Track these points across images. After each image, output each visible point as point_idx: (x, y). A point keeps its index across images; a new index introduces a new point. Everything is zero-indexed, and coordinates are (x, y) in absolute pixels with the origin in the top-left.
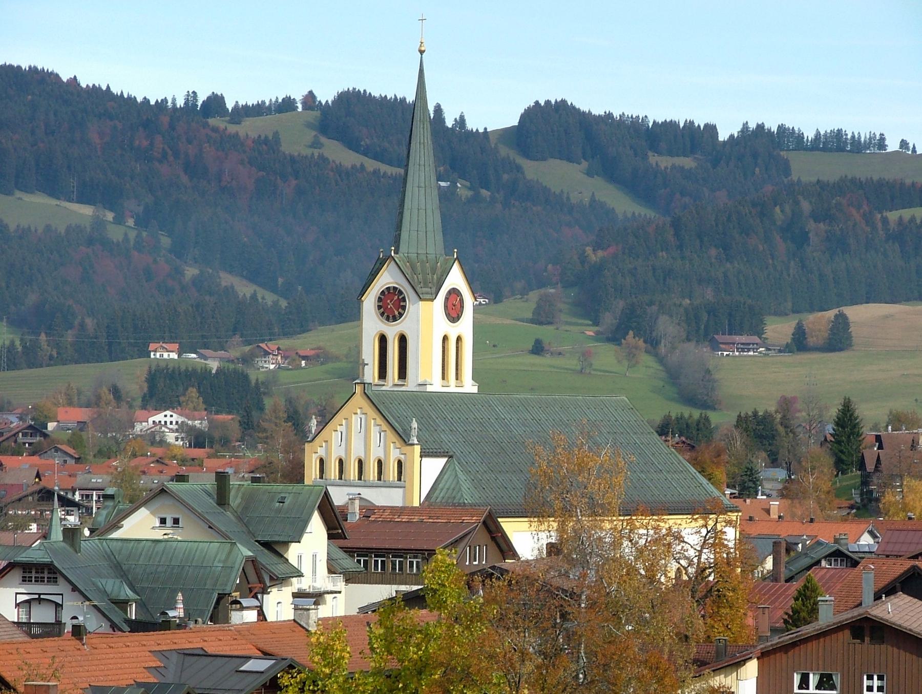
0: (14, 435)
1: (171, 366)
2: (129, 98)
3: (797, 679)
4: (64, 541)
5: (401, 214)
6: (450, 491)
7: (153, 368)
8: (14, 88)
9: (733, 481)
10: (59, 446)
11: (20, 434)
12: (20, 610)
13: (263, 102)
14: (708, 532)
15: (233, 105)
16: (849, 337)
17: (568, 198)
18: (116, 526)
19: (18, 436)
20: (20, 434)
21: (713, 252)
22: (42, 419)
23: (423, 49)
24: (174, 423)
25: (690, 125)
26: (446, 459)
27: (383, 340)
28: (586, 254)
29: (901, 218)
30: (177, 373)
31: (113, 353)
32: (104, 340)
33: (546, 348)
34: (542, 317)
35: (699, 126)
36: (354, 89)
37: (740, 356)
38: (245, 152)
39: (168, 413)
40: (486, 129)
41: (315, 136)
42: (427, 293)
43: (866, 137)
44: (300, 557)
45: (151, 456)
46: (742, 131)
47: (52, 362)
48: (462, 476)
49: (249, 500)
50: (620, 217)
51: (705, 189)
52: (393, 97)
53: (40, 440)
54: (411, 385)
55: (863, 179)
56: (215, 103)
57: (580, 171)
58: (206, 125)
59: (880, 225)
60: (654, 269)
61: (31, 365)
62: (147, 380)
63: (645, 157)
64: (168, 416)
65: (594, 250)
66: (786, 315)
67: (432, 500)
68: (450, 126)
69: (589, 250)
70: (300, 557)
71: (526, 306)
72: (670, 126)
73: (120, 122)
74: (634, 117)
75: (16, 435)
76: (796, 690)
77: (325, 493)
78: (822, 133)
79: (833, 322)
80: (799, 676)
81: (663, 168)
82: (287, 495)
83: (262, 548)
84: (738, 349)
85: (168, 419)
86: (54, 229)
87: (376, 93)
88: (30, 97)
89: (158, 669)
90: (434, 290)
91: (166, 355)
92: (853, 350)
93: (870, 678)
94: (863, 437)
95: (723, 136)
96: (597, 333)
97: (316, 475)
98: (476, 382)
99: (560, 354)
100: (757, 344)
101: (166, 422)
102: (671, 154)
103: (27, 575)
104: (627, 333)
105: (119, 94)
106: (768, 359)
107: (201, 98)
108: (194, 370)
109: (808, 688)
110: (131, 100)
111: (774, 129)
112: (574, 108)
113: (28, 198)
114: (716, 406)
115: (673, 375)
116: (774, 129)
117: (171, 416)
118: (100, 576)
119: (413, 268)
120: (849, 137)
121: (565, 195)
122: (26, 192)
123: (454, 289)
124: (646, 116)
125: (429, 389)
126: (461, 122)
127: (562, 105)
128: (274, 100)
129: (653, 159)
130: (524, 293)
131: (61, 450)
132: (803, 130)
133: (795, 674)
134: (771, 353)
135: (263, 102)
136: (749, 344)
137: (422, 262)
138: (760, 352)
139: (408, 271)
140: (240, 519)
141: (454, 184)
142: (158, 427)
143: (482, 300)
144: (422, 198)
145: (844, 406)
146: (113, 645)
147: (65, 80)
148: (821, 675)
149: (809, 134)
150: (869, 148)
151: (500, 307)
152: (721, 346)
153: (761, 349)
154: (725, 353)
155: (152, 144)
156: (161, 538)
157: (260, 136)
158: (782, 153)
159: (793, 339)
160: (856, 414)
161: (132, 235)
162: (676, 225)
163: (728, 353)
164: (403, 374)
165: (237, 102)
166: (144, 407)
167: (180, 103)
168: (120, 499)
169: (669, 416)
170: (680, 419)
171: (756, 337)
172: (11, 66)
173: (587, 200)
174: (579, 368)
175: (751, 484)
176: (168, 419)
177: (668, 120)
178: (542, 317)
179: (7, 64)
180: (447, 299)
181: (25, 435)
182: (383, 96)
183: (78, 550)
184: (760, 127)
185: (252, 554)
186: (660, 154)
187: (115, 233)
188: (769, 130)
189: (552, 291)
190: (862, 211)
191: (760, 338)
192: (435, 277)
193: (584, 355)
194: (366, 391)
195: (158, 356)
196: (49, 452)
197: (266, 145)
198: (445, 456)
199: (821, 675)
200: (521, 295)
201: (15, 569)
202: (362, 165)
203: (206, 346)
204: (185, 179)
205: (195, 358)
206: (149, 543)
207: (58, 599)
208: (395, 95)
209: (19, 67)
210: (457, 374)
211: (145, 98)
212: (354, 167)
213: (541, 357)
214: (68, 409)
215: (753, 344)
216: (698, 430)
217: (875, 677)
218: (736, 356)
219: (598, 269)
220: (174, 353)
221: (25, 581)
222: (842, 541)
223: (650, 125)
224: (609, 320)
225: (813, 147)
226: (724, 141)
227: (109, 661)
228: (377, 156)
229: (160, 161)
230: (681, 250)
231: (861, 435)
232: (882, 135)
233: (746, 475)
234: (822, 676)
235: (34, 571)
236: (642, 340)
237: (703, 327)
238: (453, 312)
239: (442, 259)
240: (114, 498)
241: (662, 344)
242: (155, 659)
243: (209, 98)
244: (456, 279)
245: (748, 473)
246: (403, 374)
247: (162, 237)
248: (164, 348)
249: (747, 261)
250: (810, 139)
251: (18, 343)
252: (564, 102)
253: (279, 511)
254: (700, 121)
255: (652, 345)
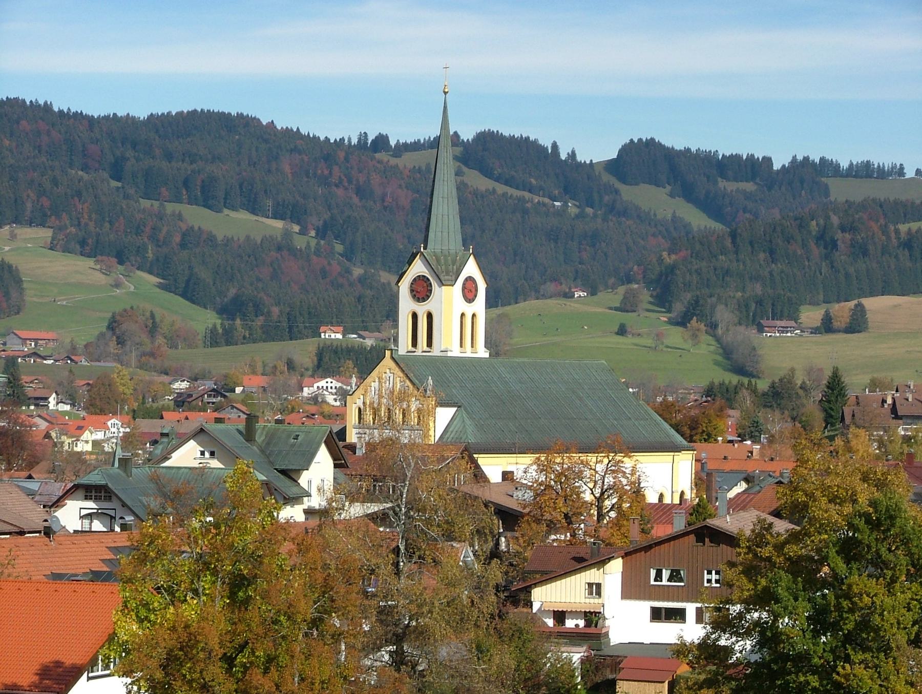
0: (201, 396)
1: (335, 344)
2: (314, 137)
3: (653, 573)
4: (119, 468)
5: (429, 219)
6: (454, 433)
7: (321, 345)
8: (225, 129)
9: (743, 431)
10: (234, 405)
11: (206, 395)
12: (84, 521)
13: (419, 140)
14: (610, 461)
15: (395, 143)
16: (865, 322)
17: (655, 215)
18: (166, 458)
19: (204, 397)
20: (206, 395)
21: (762, 256)
22: (231, 385)
23: (446, 90)
24: (334, 387)
25: (751, 157)
26: (456, 409)
27: (415, 316)
28: (662, 258)
29: (910, 229)
30: (340, 350)
31: (292, 334)
32: (285, 324)
33: (629, 330)
34: (627, 306)
35: (758, 158)
36: (489, 130)
37: (780, 337)
38: (403, 179)
39: (329, 380)
40: (591, 161)
41: (459, 166)
42: (448, 280)
43: (889, 167)
44: (310, 482)
45: (303, 412)
46: (792, 162)
47: (245, 341)
48: (468, 422)
49: (271, 437)
50: (695, 229)
51: (762, 207)
52: (520, 136)
53: (221, 400)
54: (436, 352)
55: (882, 200)
56: (381, 141)
57: (666, 194)
58: (373, 158)
59: (893, 235)
60: (715, 269)
61: (228, 343)
62: (317, 355)
63: (715, 183)
64: (329, 382)
65: (669, 254)
66: (819, 304)
67: (444, 440)
68: (563, 159)
69: (665, 254)
70: (310, 482)
71: (615, 297)
72: (735, 158)
73: (306, 156)
74: (707, 151)
75: (202, 396)
76: (652, 582)
77: (330, 431)
78: (855, 163)
79: (852, 310)
80: (655, 571)
81: (729, 191)
82: (300, 434)
83: (279, 474)
84: (778, 331)
85: (329, 385)
86: (252, 238)
87: (506, 133)
88: (237, 137)
89: (112, 561)
90: (454, 278)
91: (333, 336)
92: (869, 332)
93: (709, 573)
94: (848, 397)
95: (777, 166)
96: (669, 319)
97: (355, 421)
98: (488, 349)
99: (639, 335)
100: (794, 327)
101: (327, 387)
102: (736, 179)
103: (88, 494)
104: (692, 319)
105: (306, 134)
106: (802, 339)
107: (371, 138)
108: (353, 347)
109: (661, 581)
110: (316, 139)
111: (817, 160)
112: (660, 144)
113: (233, 214)
114: (760, 375)
115: (727, 352)
116: (817, 160)
117: (332, 382)
118: (147, 495)
119: (438, 260)
120: (876, 166)
121: (652, 212)
122: (233, 210)
123: (470, 277)
124: (717, 151)
125: (450, 354)
126: (573, 155)
127: (651, 144)
128: (427, 139)
129: (722, 184)
130: (614, 287)
131: (236, 408)
132: (839, 161)
133: (652, 570)
134: (805, 334)
135: (419, 140)
136: (787, 327)
137: (445, 256)
138: (796, 334)
139: (433, 263)
140: (263, 451)
141: (565, 205)
142: (321, 391)
143: (581, 293)
144: (446, 207)
145: (833, 373)
146: (76, 542)
147: (264, 124)
148: (672, 570)
149: (844, 164)
150: (891, 175)
151: (595, 298)
152: (766, 329)
153: (797, 331)
154: (769, 334)
155: (331, 173)
156: (198, 466)
157: (415, 167)
158: (823, 179)
159: (821, 324)
160: (843, 380)
161: (313, 243)
162: (734, 235)
163: (771, 334)
164: (430, 343)
165: (398, 141)
166: (312, 376)
167: (355, 141)
168: (174, 437)
169: (713, 382)
170: (722, 384)
171: (793, 322)
172: (223, 113)
173: (669, 216)
174: (654, 345)
175: (757, 434)
176: (329, 385)
177: (734, 154)
178: (627, 306)
179: (220, 111)
180: (464, 284)
181: (209, 396)
182: (512, 135)
183: (129, 474)
184: (806, 159)
185: (266, 479)
186: (728, 180)
187: (300, 242)
188: (813, 161)
189: (636, 286)
190: (879, 224)
191: (796, 323)
192: (455, 267)
193: (657, 335)
194: (393, 356)
195: (327, 337)
196: (227, 409)
197: (419, 173)
198: (455, 406)
199: (672, 570)
200: (612, 289)
201: (78, 490)
202: (494, 190)
203: (365, 329)
204: (355, 200)
205: (355, 338)
206: (187, 470)
207: (112, 513)
208: (521, 135)
209: (230, 114)
210: (472, 343)
211: (326, 137)
212: (487, 190)
213: (624, 338)
214: (251, 376)
215: (791, 327)
216: (735, 393)
217: (714, 572)
218: (777, 337)
219: (672, 269)
220: (339, 334)
221: (97, 499)
222: (784, 475)
223: (720, 157)
224: (679, 307)
225: (847, 175)
226: (778, 170)
227: (71, 554)
228: (507, 183)
229: (336, 186)
230: (737, 254)
231: (846, 396)
232: (901, 165)
233: (753, 426)
234: (672, 571)
235: (93, 492)
236: (703, 324)
237: (751, 314)
238: (469, 293)
239: (460, 253)
240: (168, 436)
241: (720, 328)
242: (110, 553)
243: (376, 137)
244: (471, 269)
245: (755, 425)
246: (430, 343)
247: (336, 245)
248: (331, 330)
249: (788, 263)
250: (845, 168)
251: (219, 327)
252: (652, 140)
253: (293, 445)
254: (759, 155)
255: (711, 327)
